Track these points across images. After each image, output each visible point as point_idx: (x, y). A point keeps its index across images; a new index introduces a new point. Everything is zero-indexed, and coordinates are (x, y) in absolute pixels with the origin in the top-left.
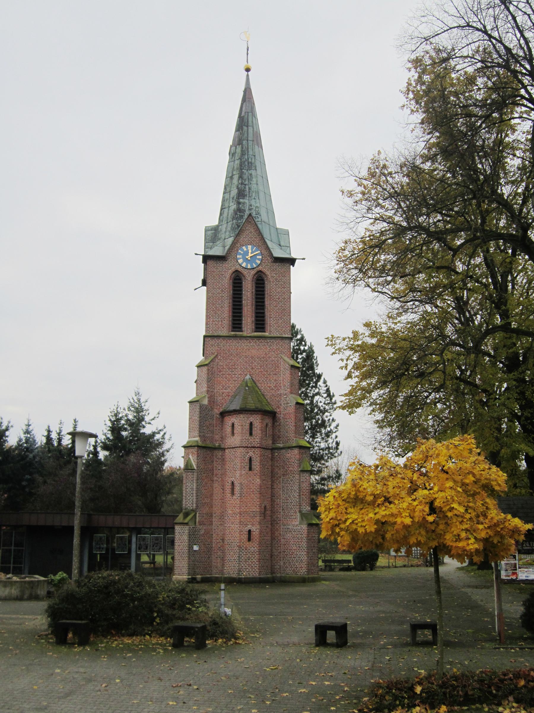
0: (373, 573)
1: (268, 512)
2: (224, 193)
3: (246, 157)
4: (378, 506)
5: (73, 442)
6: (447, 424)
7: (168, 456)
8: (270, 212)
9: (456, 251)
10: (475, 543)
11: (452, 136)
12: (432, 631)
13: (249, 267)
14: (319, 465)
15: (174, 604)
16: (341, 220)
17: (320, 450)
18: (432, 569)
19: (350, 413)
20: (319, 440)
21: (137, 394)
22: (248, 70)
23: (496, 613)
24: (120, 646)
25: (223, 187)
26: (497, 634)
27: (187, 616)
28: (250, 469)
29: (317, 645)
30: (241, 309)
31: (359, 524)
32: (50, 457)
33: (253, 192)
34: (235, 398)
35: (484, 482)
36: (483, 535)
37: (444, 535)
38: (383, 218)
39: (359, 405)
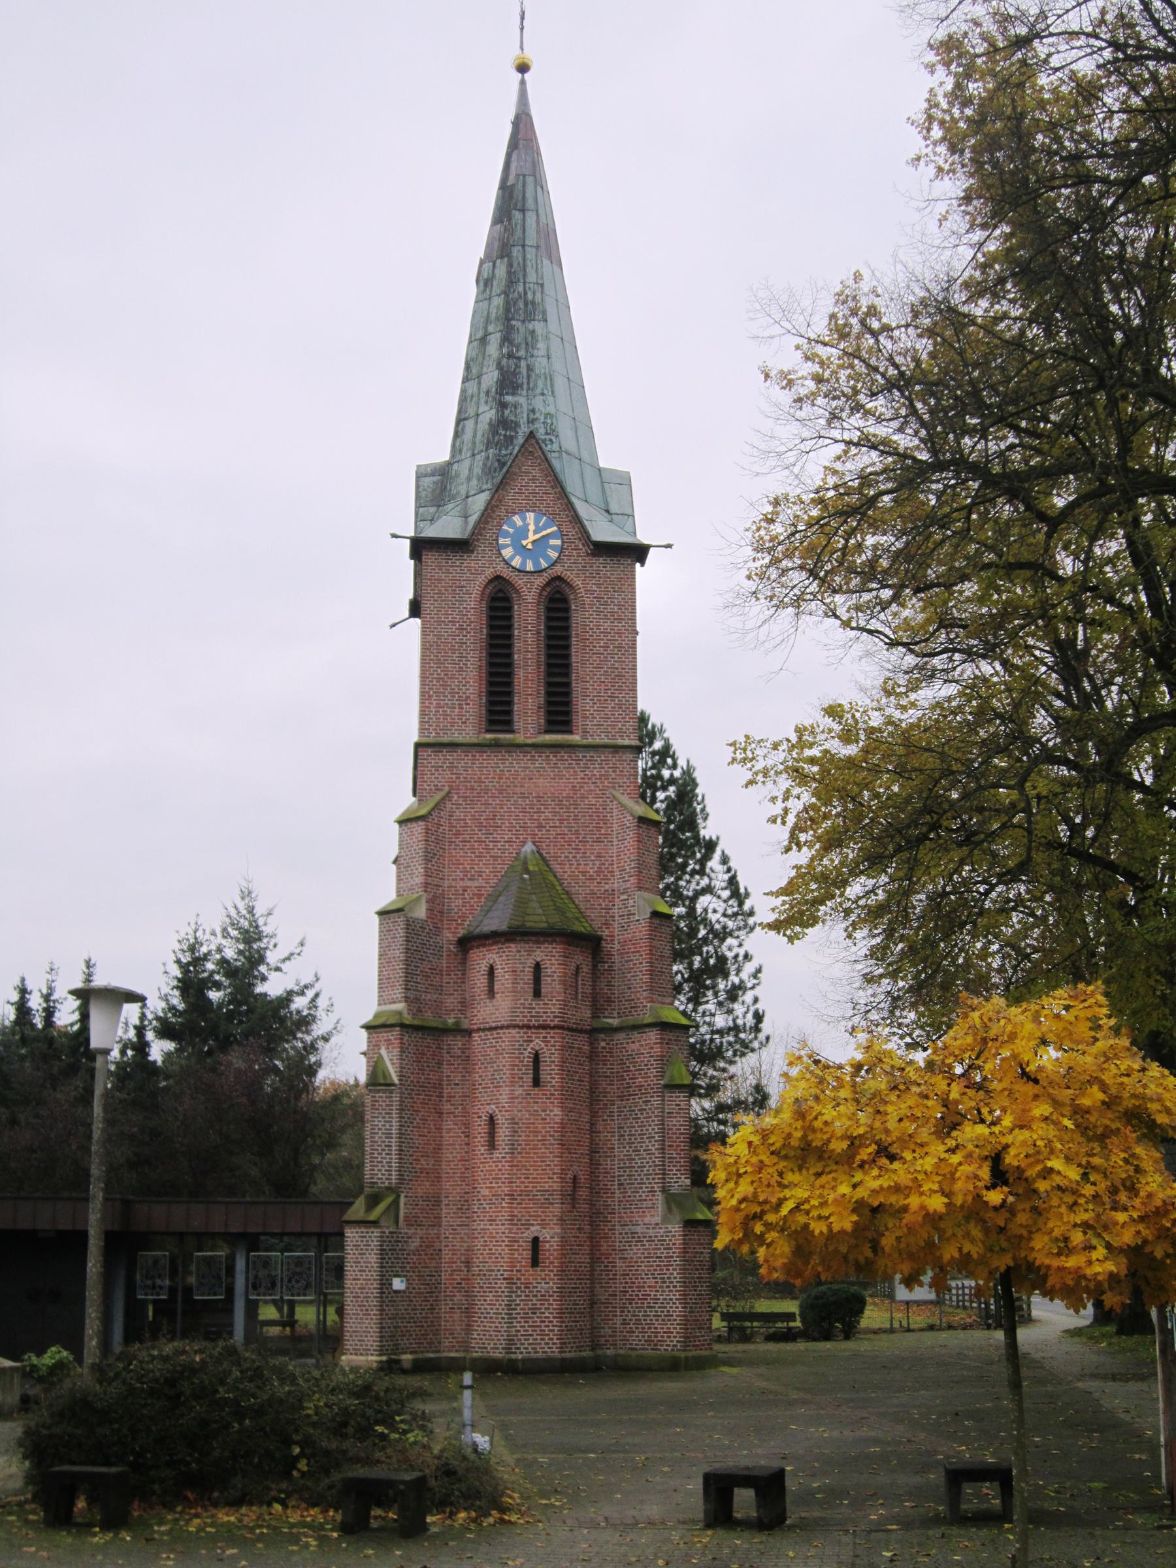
0: (850, 1345)
1: (583, 1193)
2: (466, 380)
3: (521, 289)
4: (861, 1166)
5: (85, 1017)
6: (1036, 964)
7: (326, 1052)
8: (583, 427)
9: (1055, 522)
10: (1106, 1258)
11: (1042, 231)
12: (1001, 1485)
13: (530, 567)
14: (711, 1072)
15: (345, 1424)
16: (763, 446)
17: (713, 1032)
18: (1000, 1335)
19: (791, 939)
20: (711, 1007)
21: (246, 894)
22: (523, 68)
23: (1162, 1439)
24: (208, 1529)
25: (463, 365)
26: (1164, 1491)
27: (378, 1455)
28: (536, 1082)
29: (709, 1525)
30: (510, 675)
31: (814, 1213)
32: (23, 1058)
33: (539, 376)
34: (495, 902)
35: (1129, 1103)
36: (1127, 1237)
37: (1030, 1239)
38: (869, 441)
39: (814, 921)
